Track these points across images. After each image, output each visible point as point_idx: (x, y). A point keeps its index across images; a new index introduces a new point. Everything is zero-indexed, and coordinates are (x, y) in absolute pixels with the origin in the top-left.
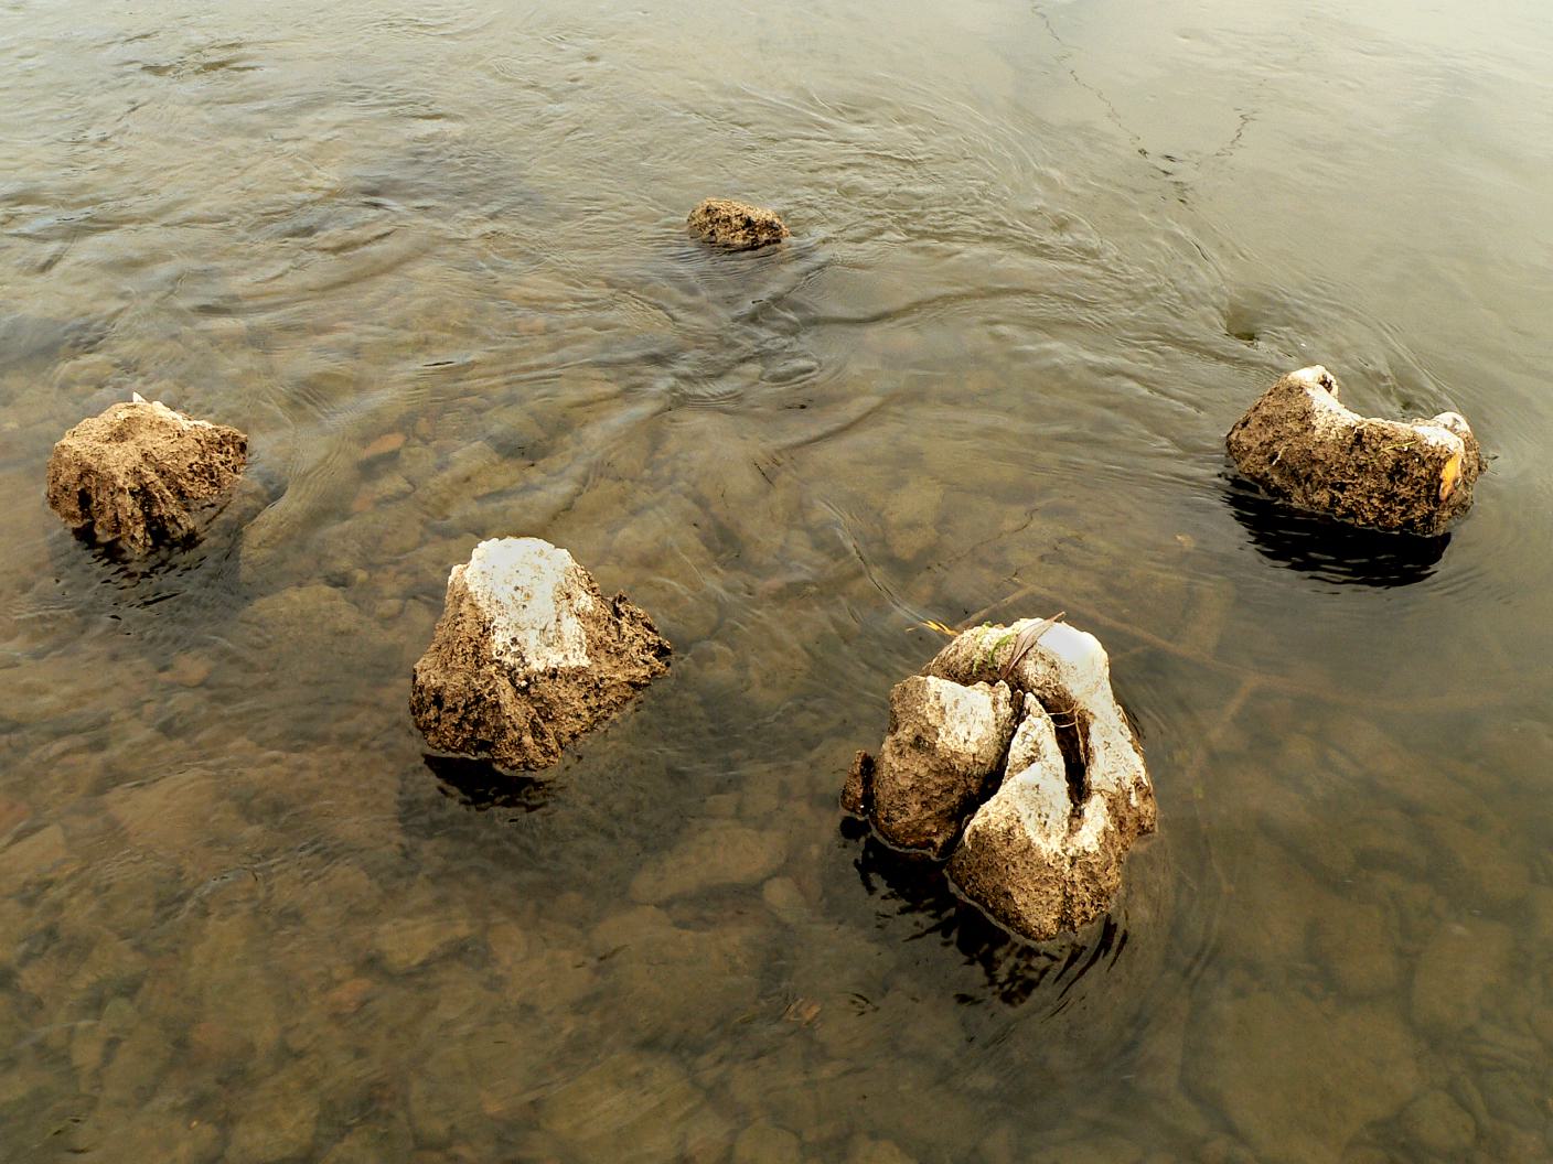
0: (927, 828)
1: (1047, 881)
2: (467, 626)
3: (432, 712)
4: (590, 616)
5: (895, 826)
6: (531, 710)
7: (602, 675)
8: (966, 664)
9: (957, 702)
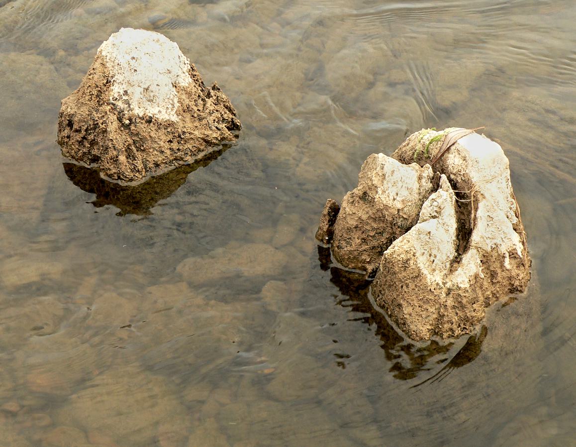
0: (363, 257)
1: (428, 301)
2: (96, 77)
3: (66, 131)
4: (184, 89)
5: (342, 252)
6: (129, 140)
7: (185, 130)
8: (411, 152)
9: (393, 172)
